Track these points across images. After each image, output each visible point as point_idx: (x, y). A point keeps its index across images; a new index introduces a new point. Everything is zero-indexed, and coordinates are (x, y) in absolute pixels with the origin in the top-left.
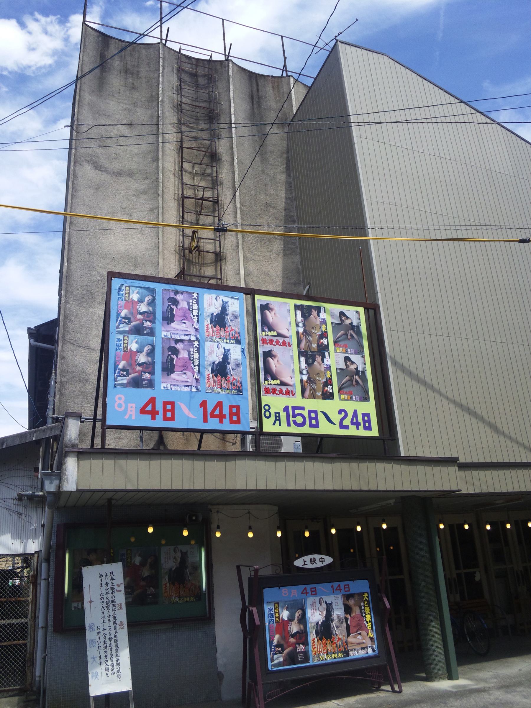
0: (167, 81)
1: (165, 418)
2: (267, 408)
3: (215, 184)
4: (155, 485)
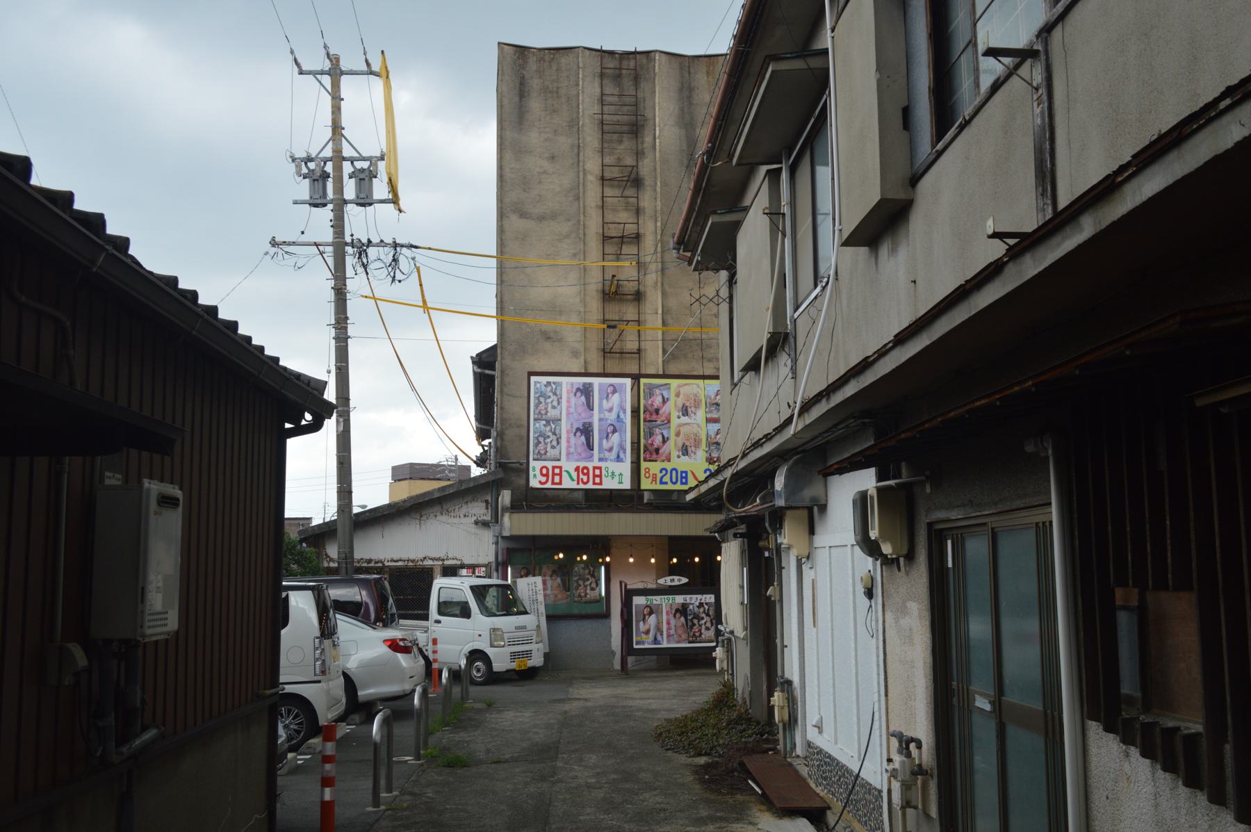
0: (589, 91)
1: (594, 483)
2: (597, 472)
3: (638, 211)
4: (559, 532)
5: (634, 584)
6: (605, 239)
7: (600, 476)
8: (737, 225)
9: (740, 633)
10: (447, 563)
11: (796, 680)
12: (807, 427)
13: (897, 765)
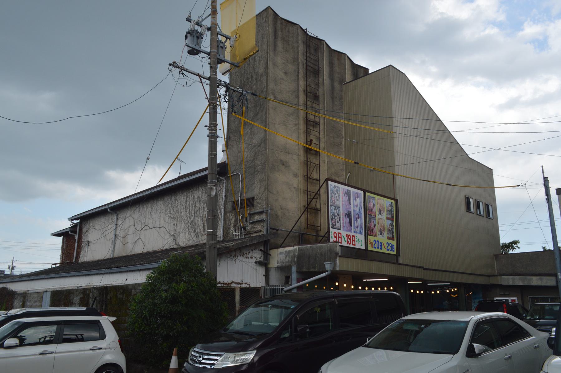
7: (354, 241)
10: (243, 286)
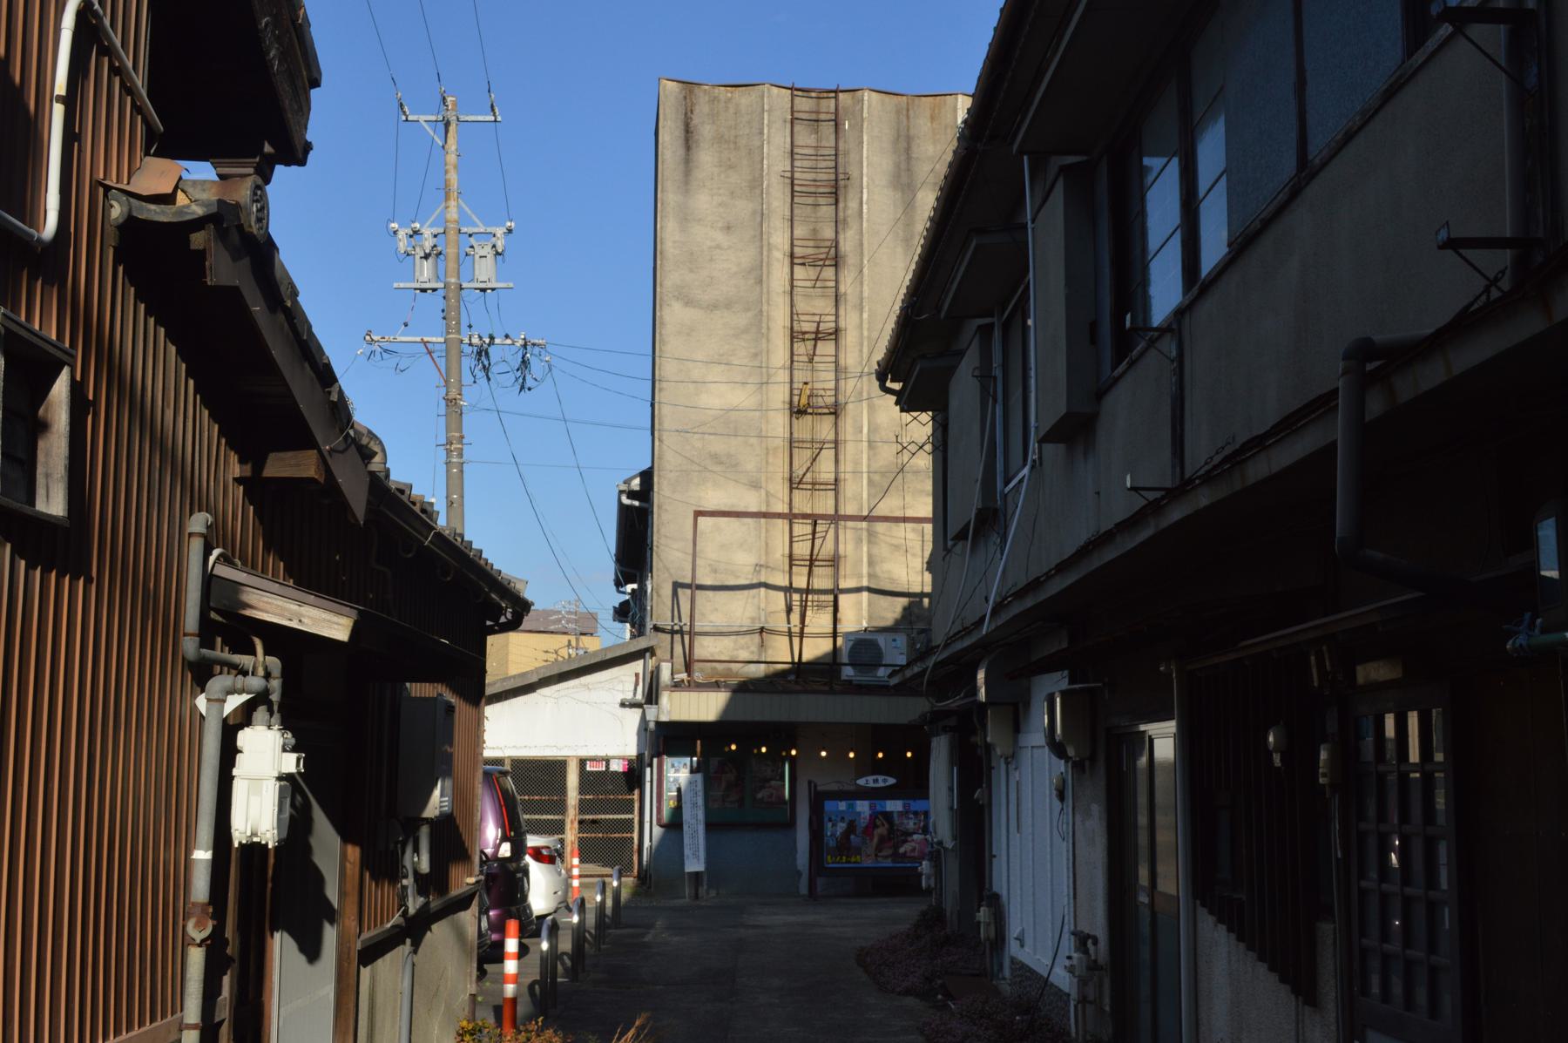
5: (826, 784)
6: (794, 336)
8: (951, 370)
9: (949, 844)
11: (1004, 893)
12: (997, 628)
13: (1075, 962)
